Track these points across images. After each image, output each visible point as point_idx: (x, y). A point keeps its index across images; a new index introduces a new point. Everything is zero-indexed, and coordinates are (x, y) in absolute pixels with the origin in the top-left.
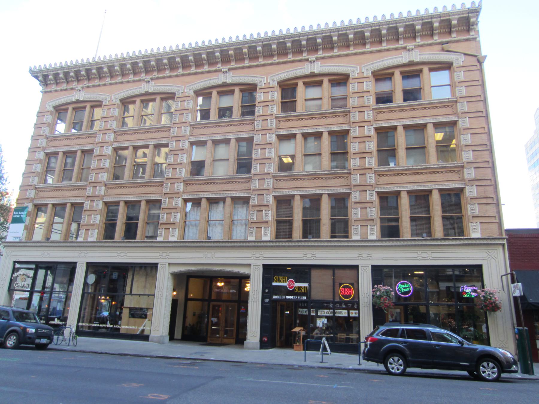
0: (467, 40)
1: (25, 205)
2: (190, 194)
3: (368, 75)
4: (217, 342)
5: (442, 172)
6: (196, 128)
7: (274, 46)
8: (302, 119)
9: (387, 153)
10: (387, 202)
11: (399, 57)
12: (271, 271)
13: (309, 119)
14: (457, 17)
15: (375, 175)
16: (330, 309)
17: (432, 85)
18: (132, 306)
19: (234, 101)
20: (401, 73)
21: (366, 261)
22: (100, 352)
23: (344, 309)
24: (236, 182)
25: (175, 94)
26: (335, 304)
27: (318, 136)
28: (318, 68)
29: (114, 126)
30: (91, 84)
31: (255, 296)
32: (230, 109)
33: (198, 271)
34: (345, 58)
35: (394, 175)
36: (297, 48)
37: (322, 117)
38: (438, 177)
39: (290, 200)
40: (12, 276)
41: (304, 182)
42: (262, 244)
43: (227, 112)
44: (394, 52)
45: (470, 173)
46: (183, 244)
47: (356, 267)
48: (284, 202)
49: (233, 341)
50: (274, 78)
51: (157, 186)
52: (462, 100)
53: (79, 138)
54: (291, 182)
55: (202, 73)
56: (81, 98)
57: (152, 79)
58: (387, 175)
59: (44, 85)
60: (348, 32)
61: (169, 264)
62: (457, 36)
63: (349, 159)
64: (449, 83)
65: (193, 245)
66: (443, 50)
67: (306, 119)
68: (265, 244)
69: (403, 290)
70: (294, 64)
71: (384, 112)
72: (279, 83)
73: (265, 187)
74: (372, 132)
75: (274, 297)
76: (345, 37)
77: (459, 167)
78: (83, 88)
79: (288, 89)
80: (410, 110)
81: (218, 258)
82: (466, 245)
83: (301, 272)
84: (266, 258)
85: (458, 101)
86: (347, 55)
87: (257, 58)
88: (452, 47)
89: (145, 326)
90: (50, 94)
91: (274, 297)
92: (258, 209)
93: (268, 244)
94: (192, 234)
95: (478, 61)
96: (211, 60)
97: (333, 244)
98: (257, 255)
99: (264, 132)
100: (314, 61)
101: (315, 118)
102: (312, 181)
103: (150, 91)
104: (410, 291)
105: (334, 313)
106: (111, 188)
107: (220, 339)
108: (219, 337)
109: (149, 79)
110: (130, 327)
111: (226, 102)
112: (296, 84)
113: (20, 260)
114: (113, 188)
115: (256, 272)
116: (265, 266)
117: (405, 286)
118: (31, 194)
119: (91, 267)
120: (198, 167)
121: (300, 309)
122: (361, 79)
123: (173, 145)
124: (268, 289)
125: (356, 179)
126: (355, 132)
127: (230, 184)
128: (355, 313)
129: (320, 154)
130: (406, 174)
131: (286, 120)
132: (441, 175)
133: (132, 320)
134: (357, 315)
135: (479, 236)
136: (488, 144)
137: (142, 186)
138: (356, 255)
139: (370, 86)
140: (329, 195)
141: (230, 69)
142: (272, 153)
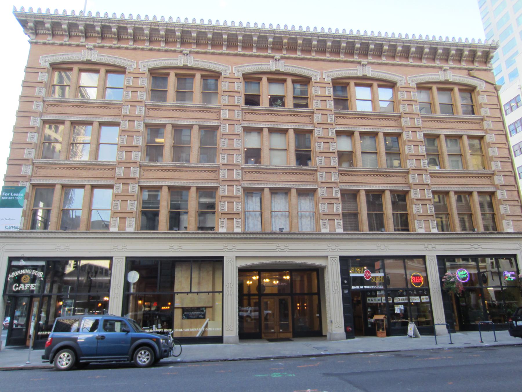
0: (485, 70)
1: (20, 184)
2: (260, 182)
3: (145, 72)
4: (273, 337)
5: (478, 177)
6: (249, 113)
7: (329, 44)
8: (358, 118)
9: (435, 158)
10: (182, 195)
11: (79, 54)
12: (346, 262)
13: (364, 118)
14: (482, 49)
15: (242, 171)
16: (404, 296)
17: (357, 98)
18: (184, 306)
19: (287, 90)
20: (176, 75)
21: (432, 251)
22: (232, 359)
23: (416, 295)
24: (300, 173)
25: (125, 68)
26: (408, 292)
27: (374, 135)
28: (282, 66)
29: (144, 99)
30: (42, 41)
31: (230, 289)
32: (282, 98)
33: (267, 264)
34: (392, 67)
35: (443, 177)
36: (349, 49)
37: (376, 119)
38: (272, 177)
39: (381, 195)
40: (7, 277)
41: (367, 177)
42: (320, 237)
43: (279, 101)
44: (432, 69)
45: (498, 180)
46: (247, 237)
47: (423, 257)
48: (350, 196)
49: (290, 335)
50: (47, 59)
51: (208, 171)
52: (318, 112)
53: (94, 107)
54: (364, 177)
55: (251, 56)
56: (94, 59)
57: (190, 52)
58: (437, 177)
59: (33, 33)
60: (412, 45)
61: (236, 257)
62: (287, 54)
63: (217, 154)
64: (370, 99)
65: (255, 236)
66: (469, 75)
67: (361, 118)
68: (324, 237)
69: (461, 277)
70: (346, 64)
71: (429, 121)
72: (333, 80)
73: (329, 180)
74: (142, 127)
75: (353, 287)
76: (280, 41)
77: (405, 172)
78: (95, 47)
79: (341, 85)
80: (449, 122)
81: (292, 251)
82: (504, 238)
83: (370, 262)
84: (341, 251)
85: (315, 112)
86: (393, 65)
87: (309, 51)
88: (475, 73)
89: (206, 326)
90: (44, 47)
91: (353, 287)
92: (329, 201)
93: (341, 237)
94: (254, 226)
95: (495, 89)
96: (278, 46)
97: (170, 236)
98: (333, 247)
99: (132, 119)
100: (279, 60)
101: (370, 118)
102: (374, 177)
103: (189, 65)
104: (467, 277)
105: (409, 299)
106: (147, 170)
107: (276, 334)
108: (274, 333)
109: (92, 47)
110: (192, 330)
111: (277, 90)
112: (168, 74)
113: (25, 256)
114: (151, 170)
115: (334, 263)
116: (438, 256)
117: (463, 273)
118: (27, 170)
119: (133, 264)
120: (253, 154)
121: (368, 298)
122: (232, 79)
123: (125, 125)
124: (346, 281)
125: (224, 174)
126: (224, 128)
127: (293, 175)
128: (426, 299)
129: (270, 149)
130: (452, 177)
131: (343, 117)
132: (477, 179)
133: (187, 321)
134: (428, 300)
135: (511, 230)
136: (509, 157)
137: (191, 171)
138: (221, 247)
139: (240, 86)
140: (391, 191)
141: (190, 52)
142: (237, 144)
